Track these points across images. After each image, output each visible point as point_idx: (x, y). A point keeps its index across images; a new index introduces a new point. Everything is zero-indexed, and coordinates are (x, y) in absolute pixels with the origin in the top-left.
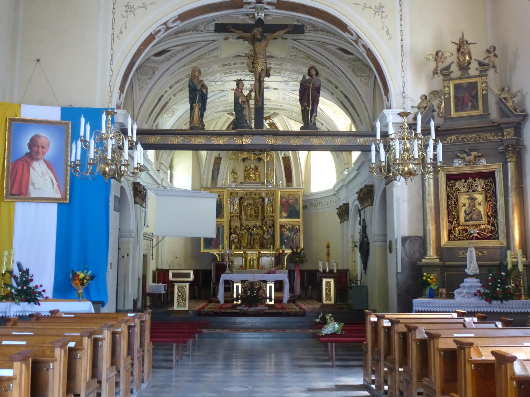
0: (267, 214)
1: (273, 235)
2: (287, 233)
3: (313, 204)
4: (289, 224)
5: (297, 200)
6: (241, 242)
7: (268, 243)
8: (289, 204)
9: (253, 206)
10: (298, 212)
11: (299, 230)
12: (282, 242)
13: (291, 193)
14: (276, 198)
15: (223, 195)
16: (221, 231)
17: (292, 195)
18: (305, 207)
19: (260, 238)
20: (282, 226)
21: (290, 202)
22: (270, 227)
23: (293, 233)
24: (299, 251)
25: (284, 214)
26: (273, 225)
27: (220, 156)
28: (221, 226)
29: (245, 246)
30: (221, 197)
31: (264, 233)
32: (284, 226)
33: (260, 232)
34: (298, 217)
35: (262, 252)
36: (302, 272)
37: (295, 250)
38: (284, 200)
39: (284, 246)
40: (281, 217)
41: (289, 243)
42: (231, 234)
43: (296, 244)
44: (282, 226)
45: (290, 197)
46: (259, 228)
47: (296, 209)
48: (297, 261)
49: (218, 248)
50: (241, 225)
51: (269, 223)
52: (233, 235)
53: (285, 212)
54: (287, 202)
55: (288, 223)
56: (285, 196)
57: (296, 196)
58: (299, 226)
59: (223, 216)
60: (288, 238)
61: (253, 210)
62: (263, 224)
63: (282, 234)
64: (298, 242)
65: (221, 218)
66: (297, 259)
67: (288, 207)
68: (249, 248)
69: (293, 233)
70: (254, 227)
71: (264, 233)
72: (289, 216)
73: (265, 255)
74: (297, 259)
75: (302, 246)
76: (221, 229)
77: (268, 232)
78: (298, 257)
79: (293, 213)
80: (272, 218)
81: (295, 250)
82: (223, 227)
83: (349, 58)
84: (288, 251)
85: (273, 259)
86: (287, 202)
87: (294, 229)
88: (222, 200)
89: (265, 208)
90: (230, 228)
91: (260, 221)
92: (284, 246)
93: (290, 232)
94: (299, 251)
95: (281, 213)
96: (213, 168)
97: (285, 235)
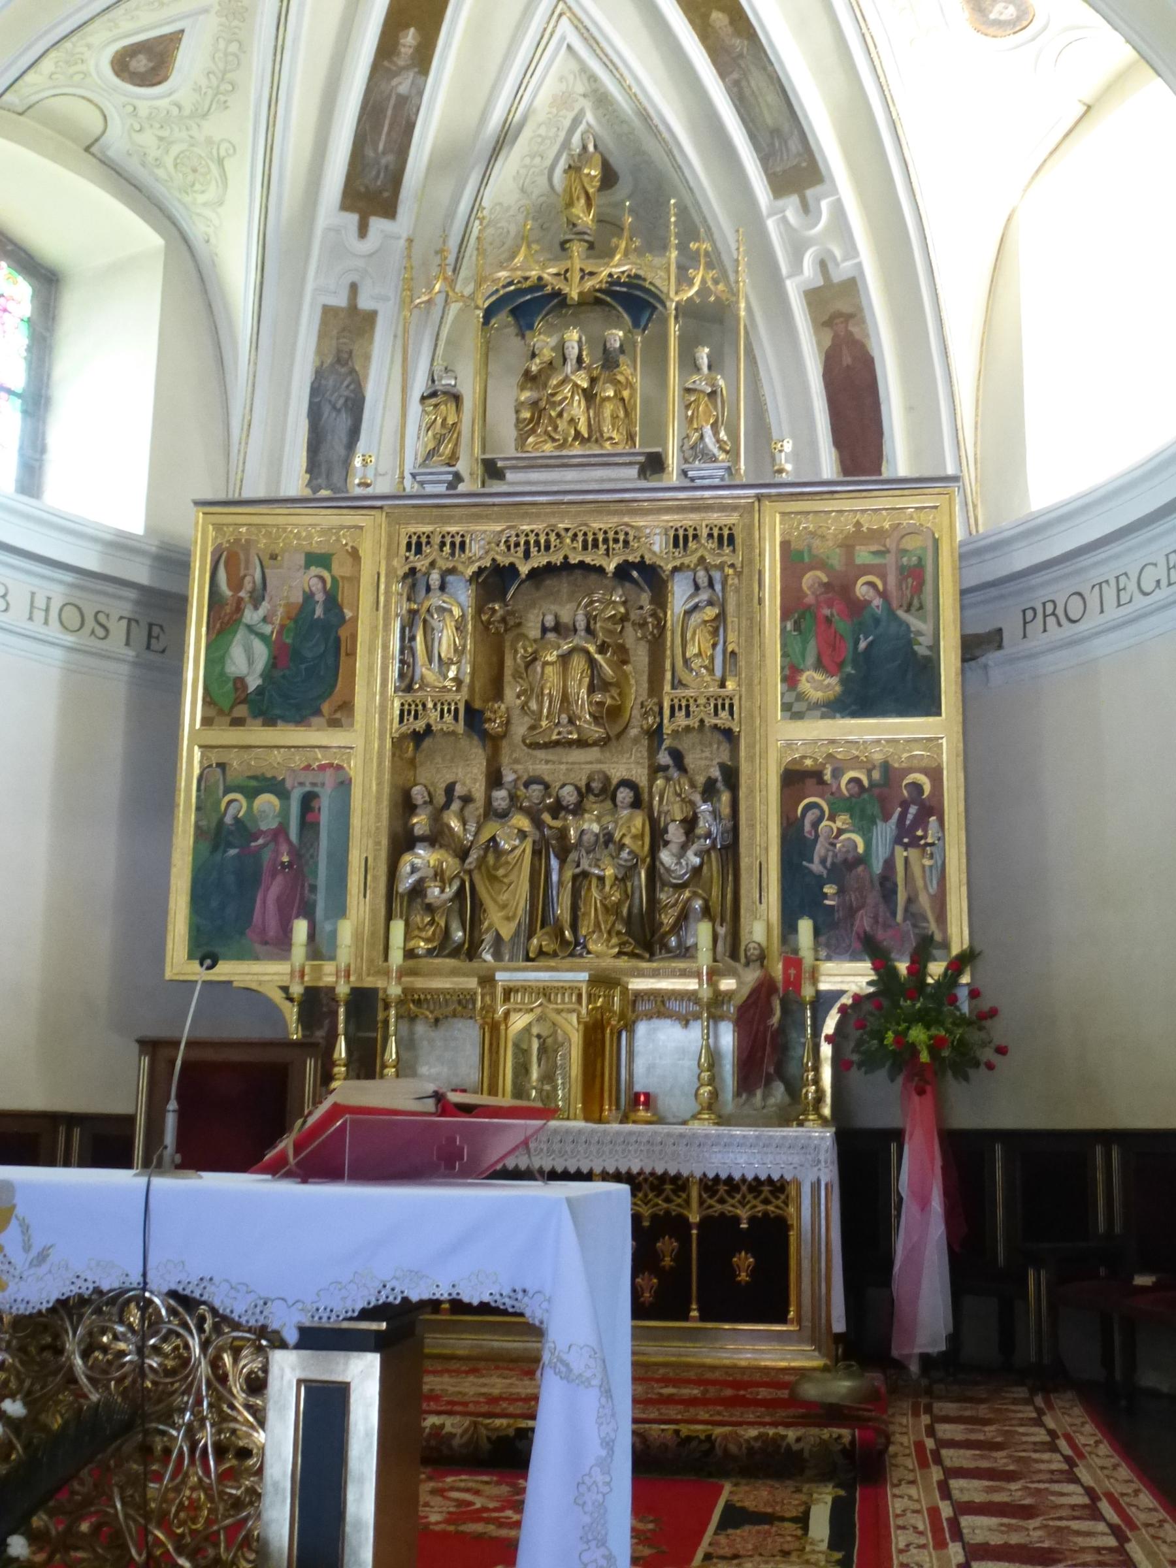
0: (677, 684)
1: (729, 851)
2: (837, 834)
3: (1051, 613)
4: (855, 762)
5: (916, 577)
6: (478, 906)
7: (684, 916)
8: (856, 607)
9: (579, 640)
10: (929, 667)
11: (931, 809)
12: (800, 896)
13: (867, 523)
14: (750, 571)
15: (355, 555)
16: (324, 819)
17: (878, 535)
18: (974, 647)
19: (625, 877)
20: (796, 779)
21: (861, 590)
22: (709, 791)
23: (885, 831)
24: (936, 969)
25: (817, 684)
26: (731, 776)
27: (364, 303)
28: (329, 777)
29: (507, 931)
30: (341, 568)
31: (658, 838)
32: (816, 775)
33: (631, 826)
34: (924, 700)
35: (638, 984)
36: (965, 1154)
37: (903, 967)
38: (810, 580)
39: (805, 927)
40: (793, 711)
41: (852, 912)
42: (402, 842)
43: (914, 916)
44: (796, 779)
45: (863, 556)
46: (624, 795)
47: (907, 640)
48: (913, 1050)
49: (282, 945)
50: (494, 779)
51: (705, 761)
52: (423, 857)
53: (819, 666)
54: (839, 589)
55: (840, 752)
56: (824, 548)
57: (910, 543)
58: (935, 775)
59: (347, 706)
60: (846, 867)
61: (578, 664)
62: (656, 770)
63: (795, 844)
64: (924, 901)
65: (334, 723)
66: (918, 1034)
67: (842, 626)
68: (541, 953)
69: (885, 831)
70: (584, 792)
71: (658, 838)
72: (859, 699)
73: (661, 1006)
74: (918, 1034)
75: (959, 938)
76: (325, 805)
77: (690, 824)
78: (926, 1019)
79: (888, 677)
80: (723, 719)
81: (903, 967)
82: (345, 785)
83: (601, 1507)
84: (849, 977)
85: (727, 1038)
86: (839, 589)
87: (899, 802)
88: (344, 597)
89: (672, 639)
90: (405, 805)
91: (641, 752)
92: (805, 927)
93: (865, 825)
94: (936, 969)
95: (790, 678)
96: (316, 390)
97: (820, 850)
